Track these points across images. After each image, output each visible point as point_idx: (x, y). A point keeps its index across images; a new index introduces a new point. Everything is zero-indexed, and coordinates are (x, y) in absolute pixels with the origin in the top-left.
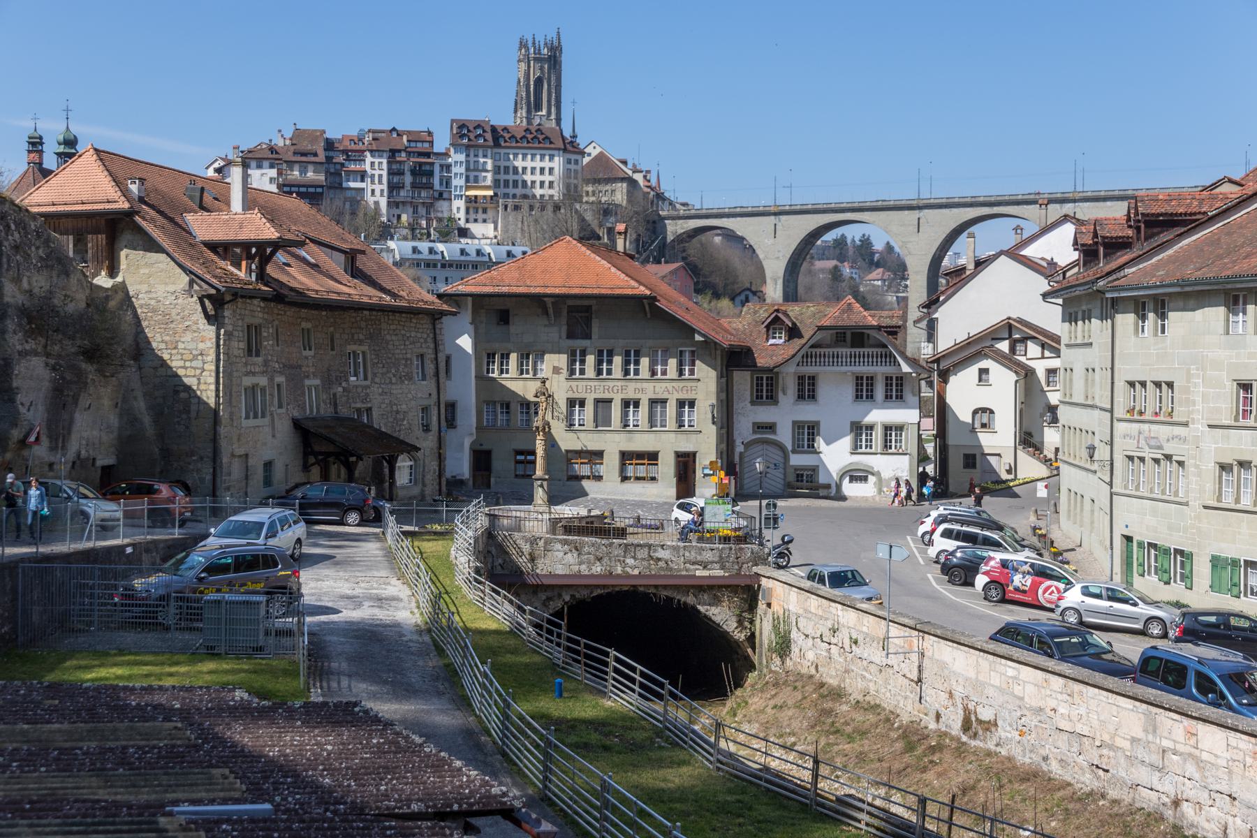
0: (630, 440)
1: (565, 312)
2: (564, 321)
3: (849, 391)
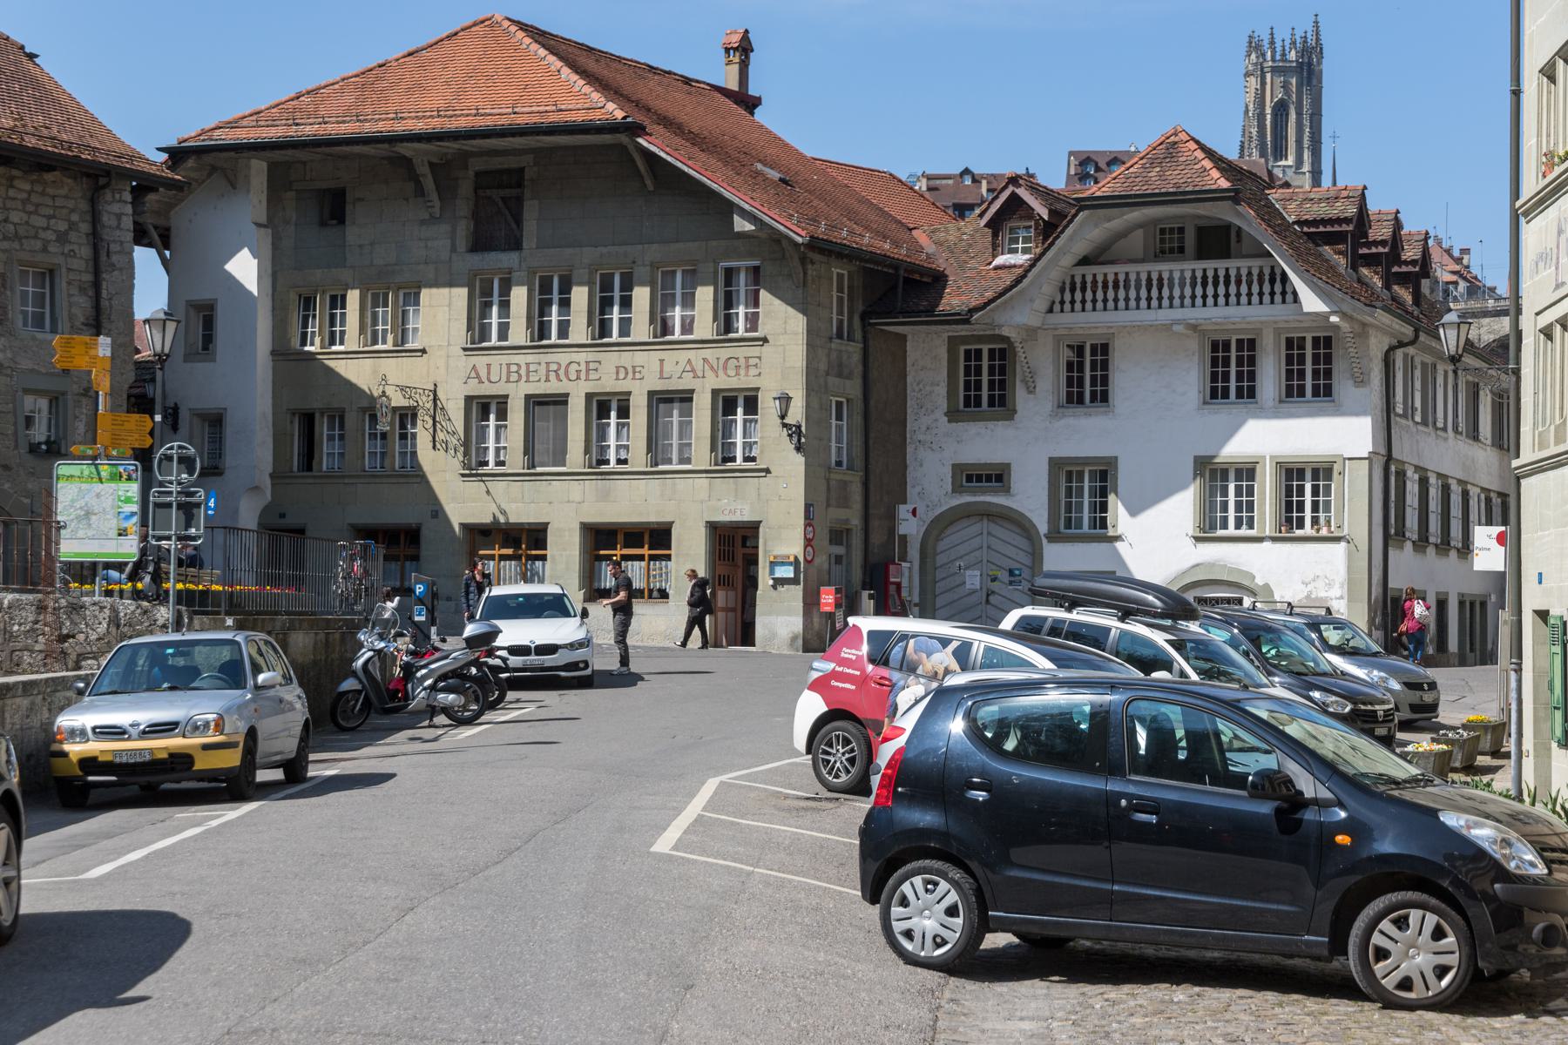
0: (604, 496)
1: (466, 188)
2: (463, 208)
3: (1191, 377)
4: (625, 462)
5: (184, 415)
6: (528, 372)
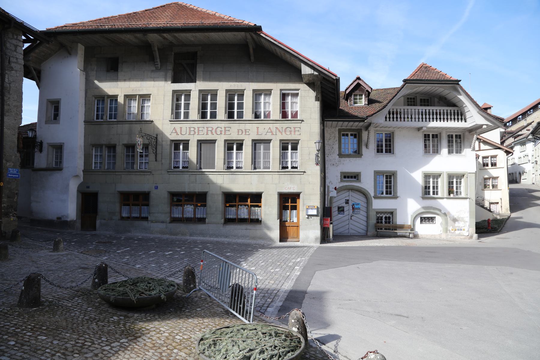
1: (172, 58)
2: (170, 67)
4: (187, 168)
5: (45, 146)
6: (199, 131)
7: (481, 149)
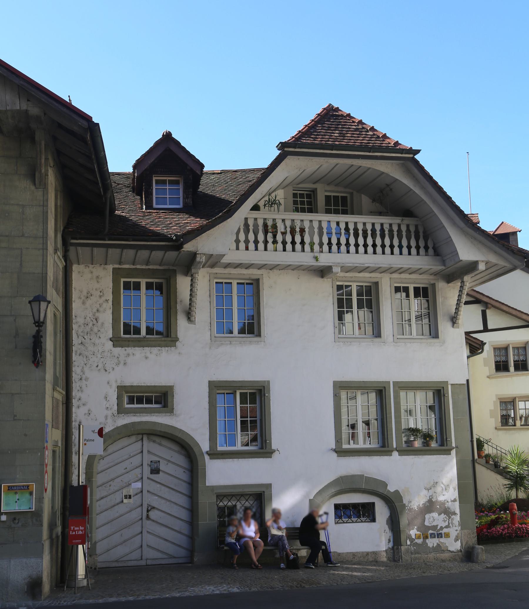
7: (490, 327)
